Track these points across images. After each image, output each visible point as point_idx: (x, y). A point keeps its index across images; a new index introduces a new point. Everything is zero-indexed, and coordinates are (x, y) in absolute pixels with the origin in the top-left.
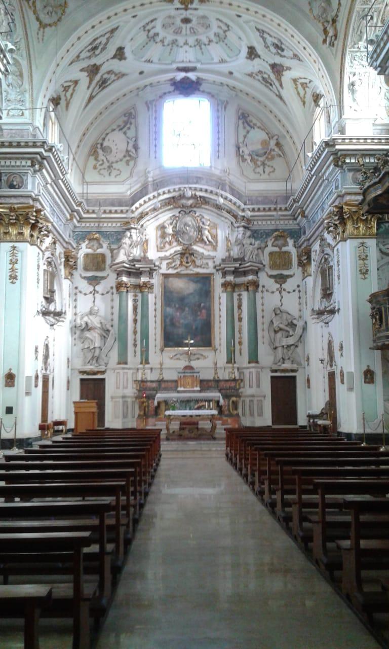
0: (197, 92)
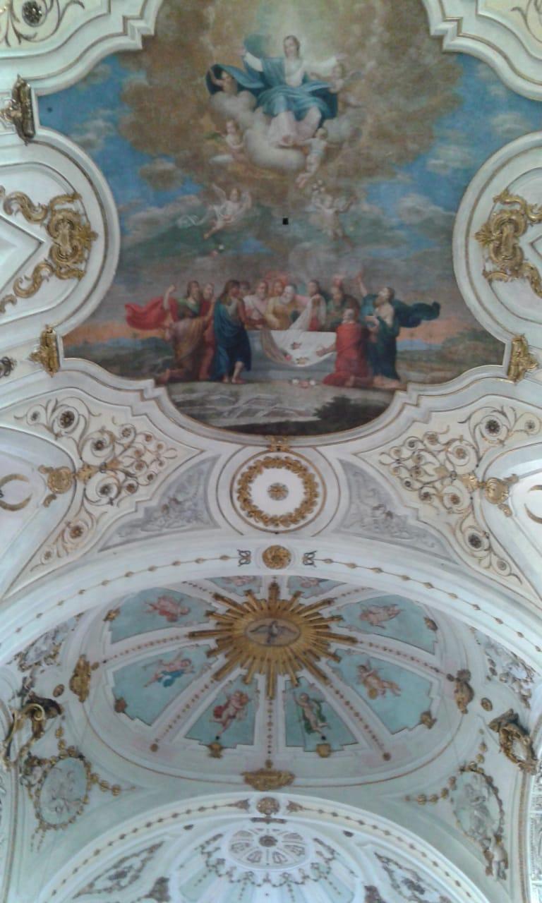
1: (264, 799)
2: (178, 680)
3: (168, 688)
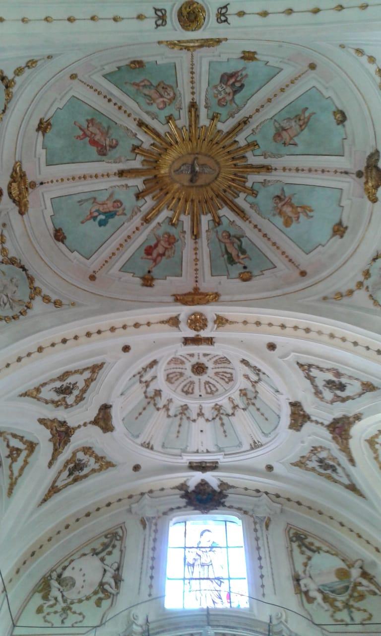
0: (221, 507)
2: (111, 220)
3: (102, 228)
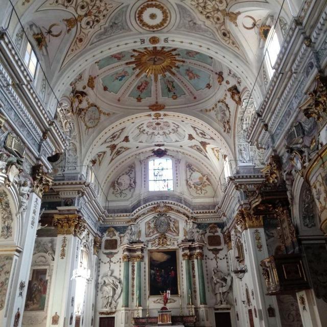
1: (156, 114)
